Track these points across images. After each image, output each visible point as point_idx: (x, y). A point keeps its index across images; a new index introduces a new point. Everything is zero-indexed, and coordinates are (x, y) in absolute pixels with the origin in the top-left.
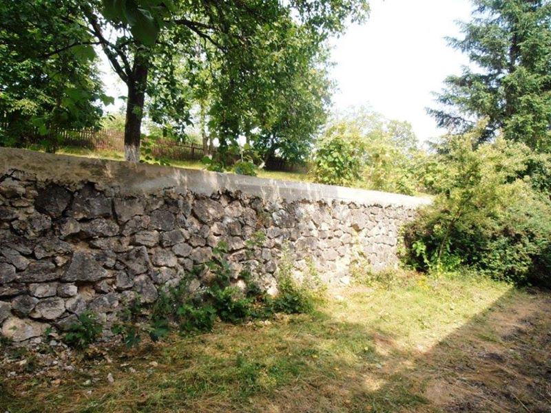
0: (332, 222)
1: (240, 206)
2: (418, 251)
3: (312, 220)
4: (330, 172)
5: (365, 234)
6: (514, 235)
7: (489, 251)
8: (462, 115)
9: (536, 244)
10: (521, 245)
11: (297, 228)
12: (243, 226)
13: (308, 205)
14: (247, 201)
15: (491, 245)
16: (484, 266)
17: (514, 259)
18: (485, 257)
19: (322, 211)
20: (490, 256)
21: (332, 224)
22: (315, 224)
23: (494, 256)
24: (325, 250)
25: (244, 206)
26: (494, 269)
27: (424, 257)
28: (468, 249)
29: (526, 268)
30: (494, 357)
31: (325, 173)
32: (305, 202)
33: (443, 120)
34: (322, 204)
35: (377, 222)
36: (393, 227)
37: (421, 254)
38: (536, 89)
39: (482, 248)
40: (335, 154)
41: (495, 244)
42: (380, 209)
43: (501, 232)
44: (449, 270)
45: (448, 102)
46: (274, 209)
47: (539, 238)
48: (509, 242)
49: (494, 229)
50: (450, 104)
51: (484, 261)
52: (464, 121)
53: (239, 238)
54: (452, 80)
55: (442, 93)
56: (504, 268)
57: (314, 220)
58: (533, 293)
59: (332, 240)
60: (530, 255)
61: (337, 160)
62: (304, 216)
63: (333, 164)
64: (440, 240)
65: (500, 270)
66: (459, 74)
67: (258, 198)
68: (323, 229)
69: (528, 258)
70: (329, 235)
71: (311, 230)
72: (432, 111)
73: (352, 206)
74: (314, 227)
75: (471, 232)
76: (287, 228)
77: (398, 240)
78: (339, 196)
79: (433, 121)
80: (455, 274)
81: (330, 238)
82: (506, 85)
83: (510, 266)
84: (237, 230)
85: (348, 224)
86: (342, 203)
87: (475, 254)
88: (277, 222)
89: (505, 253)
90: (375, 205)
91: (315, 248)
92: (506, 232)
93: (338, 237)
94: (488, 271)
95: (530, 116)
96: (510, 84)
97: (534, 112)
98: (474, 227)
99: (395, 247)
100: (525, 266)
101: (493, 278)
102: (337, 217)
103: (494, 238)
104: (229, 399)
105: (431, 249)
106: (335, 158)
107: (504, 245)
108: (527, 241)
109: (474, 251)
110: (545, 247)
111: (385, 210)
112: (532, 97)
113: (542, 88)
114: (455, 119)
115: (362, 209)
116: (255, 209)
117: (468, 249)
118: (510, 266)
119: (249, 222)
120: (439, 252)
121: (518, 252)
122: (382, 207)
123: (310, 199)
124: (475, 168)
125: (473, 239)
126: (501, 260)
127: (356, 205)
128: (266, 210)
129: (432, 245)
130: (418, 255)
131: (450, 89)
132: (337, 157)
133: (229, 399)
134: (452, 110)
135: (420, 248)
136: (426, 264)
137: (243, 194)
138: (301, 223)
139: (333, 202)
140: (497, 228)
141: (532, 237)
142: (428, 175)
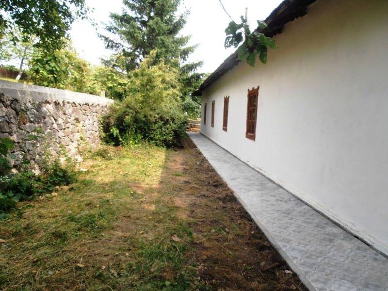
0: (64, 117)
1: (3, 107)
2: (115, 134)
3: (53, 116)
4: (49, 77)
5: (82, 125)
6: (165, 120)
7: (154, 130)
8: (121, 42)
9: (175, 124)
10: (169, 125)
11: (45, 123)
12: (9, 123)
13: (48, 105)
14: (8, 103)
15: (155, 127)
16: (152, 139)
17: (166, 133)
18: (152, 134)
19: (57, 109)
20: (154, 133)
21: (64, 119)
22: (55, 119)
23: (157, 132)
24: (62, 138)
25: (6, 107)
26: (157, 140)
27: (119, 137)
28: (143, 130)
29: (172, 138)
30: (186, 182)
31: (46, 79)
32: (47, 102)
33: (108, 44)
34: (57, 104)
35: (88, 116)
36: (96, 119)
37: (117, 135)
38: (165, 33)
39: (151, 128)
40: (53, 64)
41: (157, 126)
42: (88, 107)
43: (159, 118)
44: (136, 143)
45: (112, 31)
46: (27, 109)
47: (176, 121)
48: (163, 124)
49: (155, 117)
50: (113, 32)
51: (152, 136)
52: (122, 46)
53: (7, 134)
54: (115, 17)
55: (109, 25)
56: (162, 139)
57: (54, 116)
58: (176, 151)
59: (65, 130)
60: (173, 130)
61: (54, 69)
62: (48, 114)
63: (51, 72)
64: (128, 126)
65: (160, 140)
66: (120, 14)
67: (16, 100)
68: (59, 123)
69: (172, 132)
70: (64, 127)
71: (53, 124)
72: (101, 36)
73: (73, 104)
74: (54, 121)
75: (144, 119)
76: (38, 123)
77: (99, 127)
78: (67, 97)
79: (103, 44)
80: (140, 145)
81: (64, 129)
82: (150, 28)
83: (164, 137)
84: (5, 127)
85: (73, 118)
86: (68, 103)
87: (147, 132)
88: (32, 119)
89: (162, 130)
90: (86, 104)
91: (57, 137)
92: (161, 118)
93: (68, 128)
94: (154, 142)
95: (164, 49)
96: (152, 27)
97: (165, 47)
98: (145, 116)
99: (98, 133)
100: (171, 136)
101: (156, 145)
102: (67, 113)
103: (156, 122)
104: (89, 238)
105: (122, 131)
106: (53, 67)
107: (161, 126)
108: (171, 123)
109: (147, 130)
110: (179, 125)
111: (91, 108)
112: (164, 37)
113: (168, 33)
114: (117, 44)
115: (79, 107)
116: (15, 110)
117: (143, 130)
118: (164, 137)
119: (13, 121)
120: (128, 133)
121: (168, 129)
122: (89, 105)
123: (49, 100)
124: (150, 81)
125: (145, 123)
126: (160, 134)
127: (75, 104)
128: (23, 110)
129: (123, 129)
130: (115, 136)
131: (114, 23)
132: (55, 67)
133: (89, 238)
134: (115, 37)
135: (115, 131)
136: (121, 141)
137: (5, 96)
138: (47, 119)
139: (63, 102)
140: (157, 116)
141: (173, 120)
142: (109, 82)
